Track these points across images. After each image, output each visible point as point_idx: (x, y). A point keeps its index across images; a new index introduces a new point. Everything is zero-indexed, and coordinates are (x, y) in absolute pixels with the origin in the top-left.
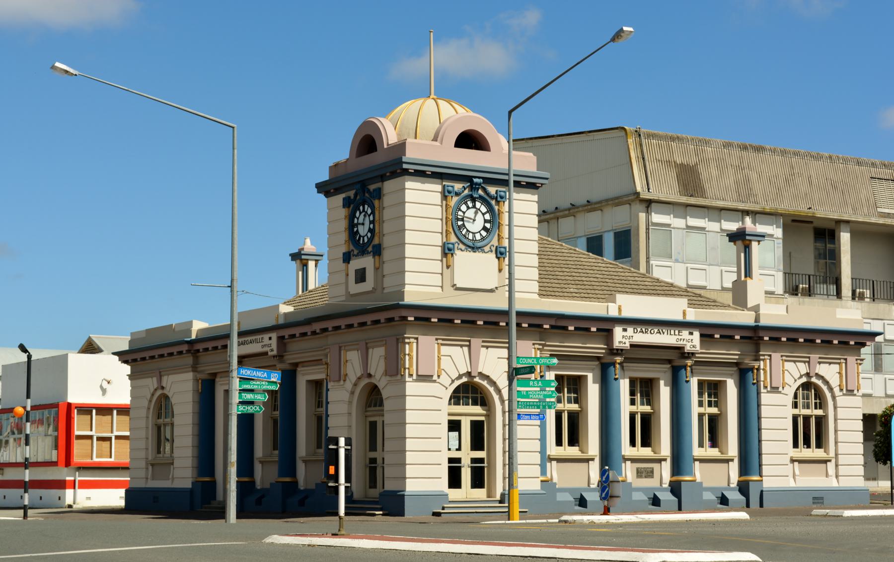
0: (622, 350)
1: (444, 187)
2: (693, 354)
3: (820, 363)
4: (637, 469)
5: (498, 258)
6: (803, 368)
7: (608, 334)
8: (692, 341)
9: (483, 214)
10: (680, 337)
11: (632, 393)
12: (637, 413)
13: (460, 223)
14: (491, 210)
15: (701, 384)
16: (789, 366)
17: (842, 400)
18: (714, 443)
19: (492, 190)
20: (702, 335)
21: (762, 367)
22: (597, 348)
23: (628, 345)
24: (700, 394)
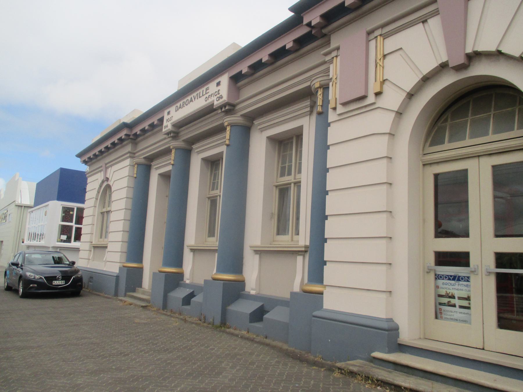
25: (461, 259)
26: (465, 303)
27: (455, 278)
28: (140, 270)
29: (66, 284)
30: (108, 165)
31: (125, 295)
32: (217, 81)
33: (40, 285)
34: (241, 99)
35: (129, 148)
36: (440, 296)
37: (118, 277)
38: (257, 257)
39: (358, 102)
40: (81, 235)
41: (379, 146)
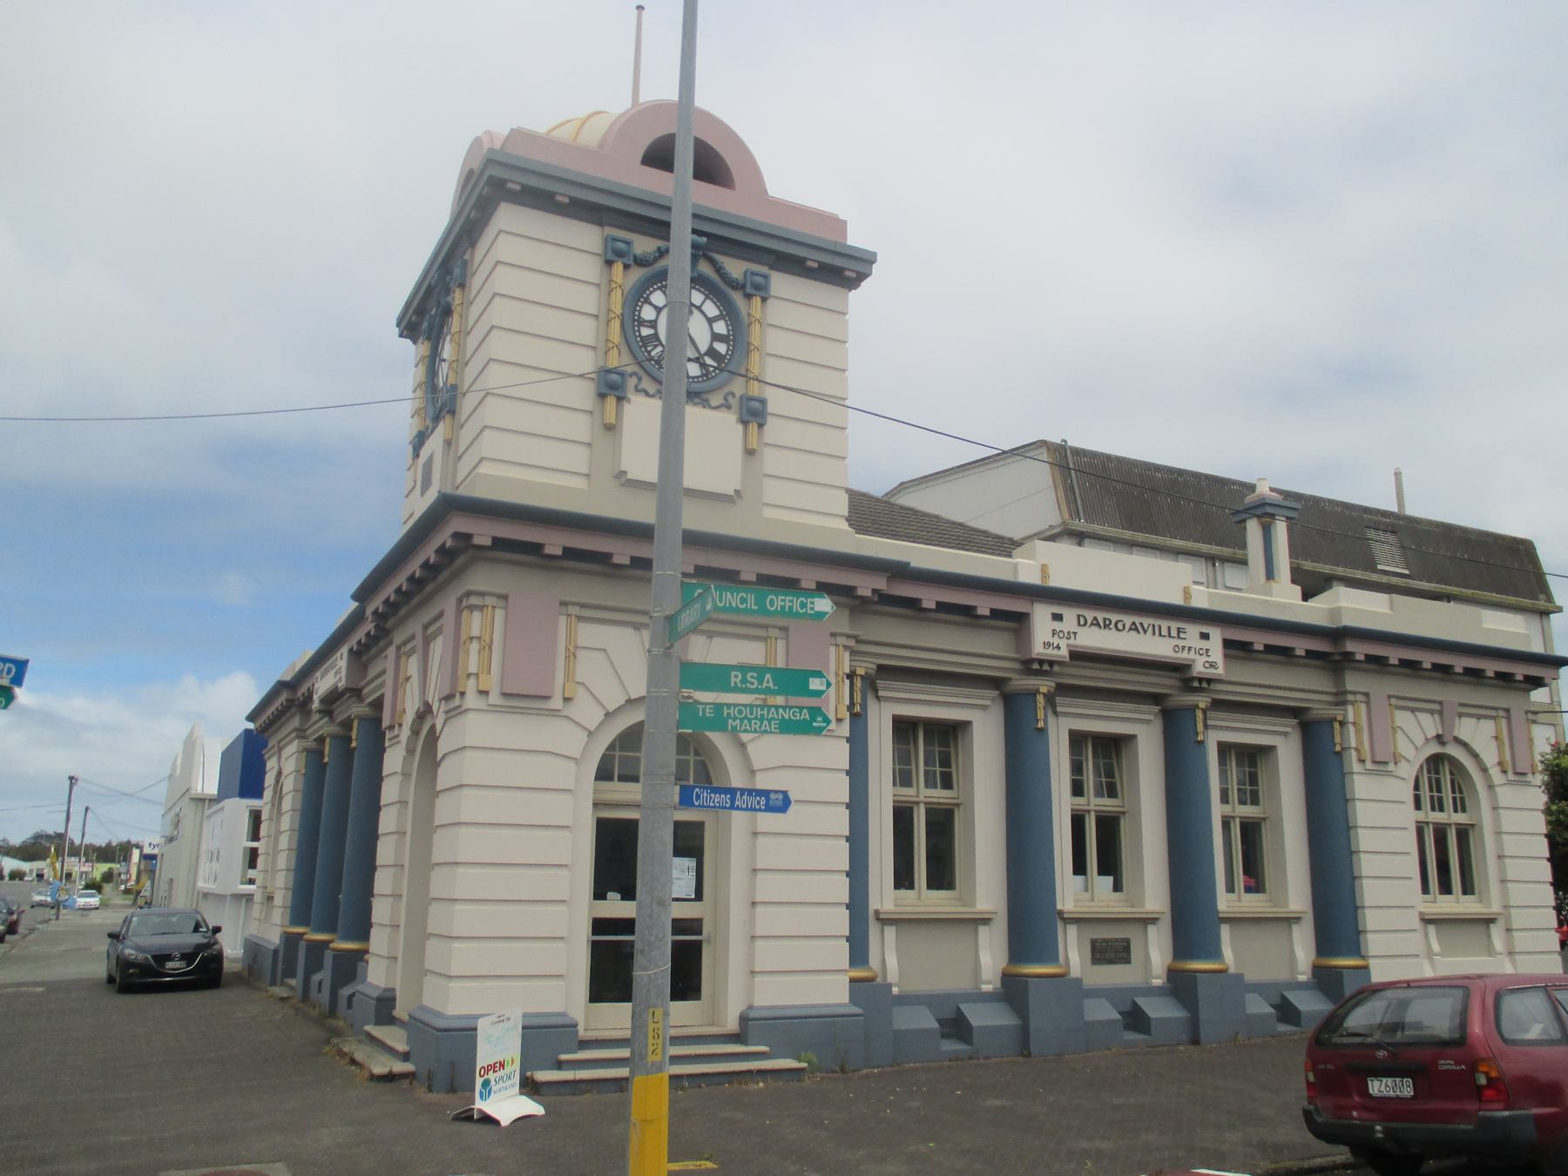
0: (1051, 663)
1: (607, 241)
2: (1209, 681)
3: (1461, 715)
4: (1094, 943)
5: (745, 423)
6: (1431, 725)
7: (1020, 621)
8: (1205, 653)
9: (710, 321)
10: (1181, 643)
11: (1077, 768)
12: (918, 803)
13: (646, 332)
14: (729, 312)
15: (1078, 740)
16: (1403, 718)
17: (1506, 795)
18: (1256, 883)
19: (736, 268)
20: (1227, 644)
21: (1351, 718)
22: (984, 649)
23: (1064, 652)
24: (903, 758)
28: (926, 764)
30: (430, 631)
33: (144, 969)
34: (370, 677)
35: (296, 722)
37: (276, 952)
40: (379, 809)
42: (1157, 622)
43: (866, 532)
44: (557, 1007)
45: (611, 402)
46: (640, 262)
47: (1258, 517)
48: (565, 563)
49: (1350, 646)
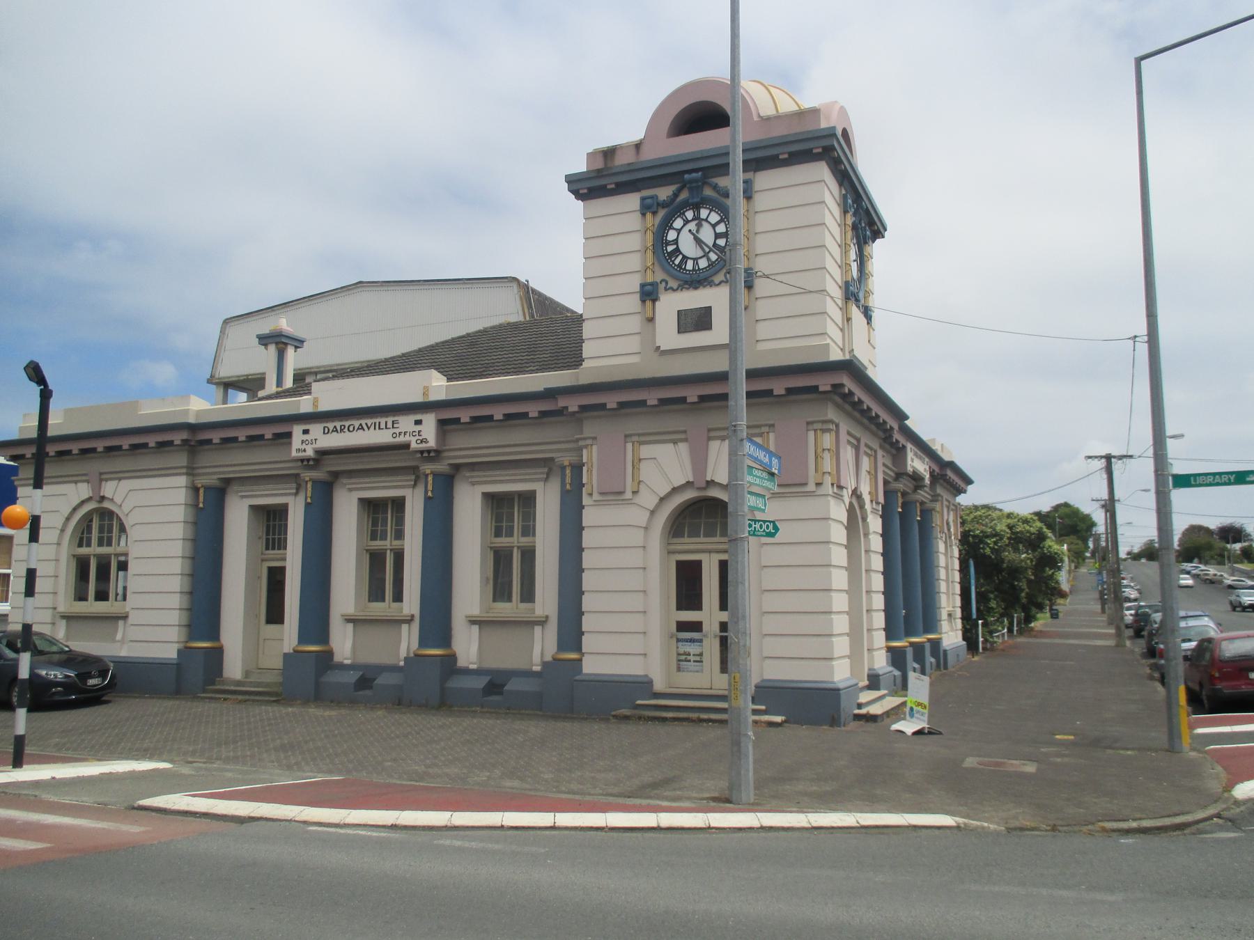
10: (397, 431)
25: (696, 626)
26: (698, 658)
27: (692, 641)
29: (104, 680)
31: (204, 691)
32: (418, 417)
36: (679, 654)
38: (64, 622)
39: (614, 495)
41: (637, 537)
42: (377, 421)
43: (457, 379)
44: (640, 672)
45: (649, 303)
46: (664, 205)
47: (277, 343)
48: (623, 411)
49: (562, 402)
